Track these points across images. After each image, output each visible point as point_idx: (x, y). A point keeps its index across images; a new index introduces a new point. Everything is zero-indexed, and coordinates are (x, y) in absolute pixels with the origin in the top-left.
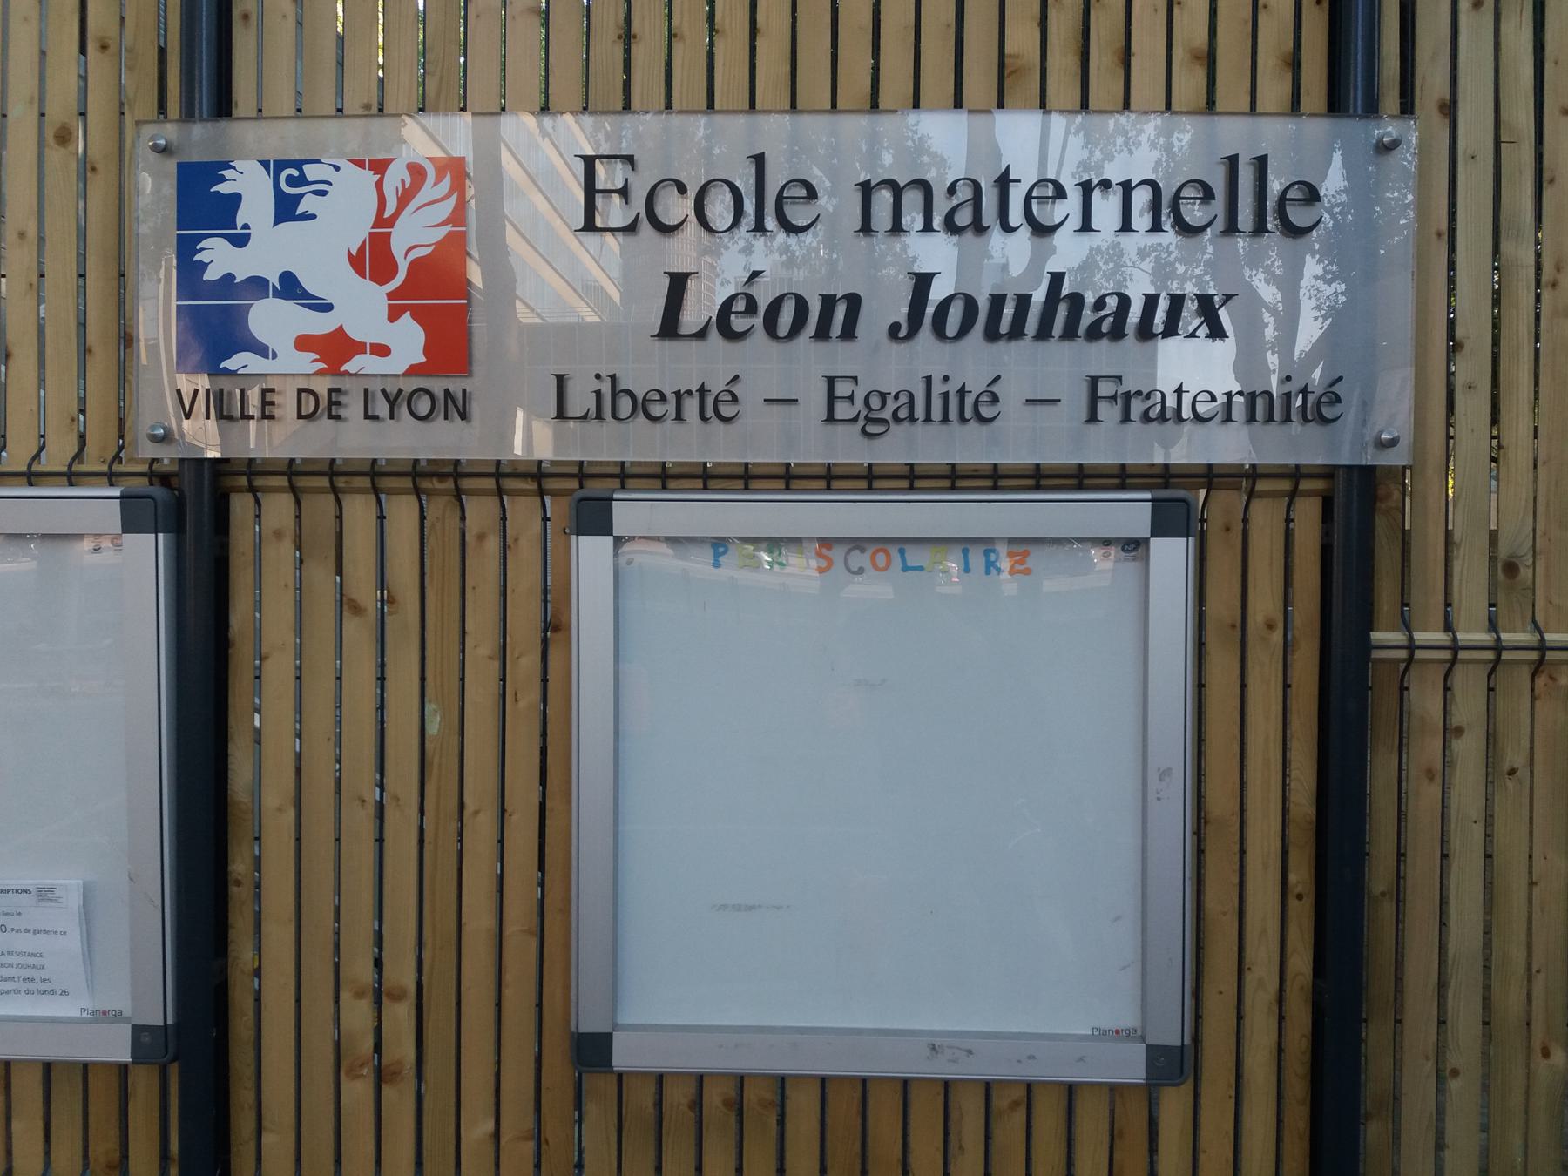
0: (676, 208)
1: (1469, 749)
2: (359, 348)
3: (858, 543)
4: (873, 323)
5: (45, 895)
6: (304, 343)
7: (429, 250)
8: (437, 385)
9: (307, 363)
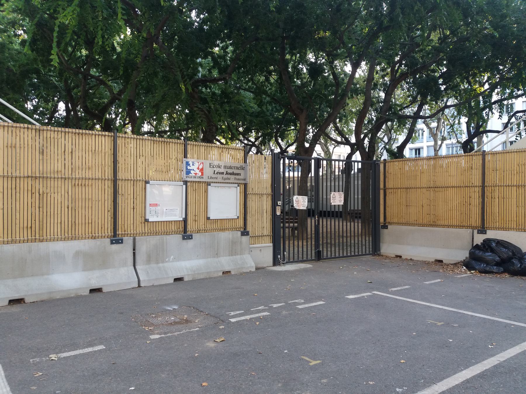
0: (214, 166)
1: (251, 199)
2: (197, 174)
3: (223, 187)
4: (224, 174)
5: (177, 209)
6: (194, 173)
7: (322, 158)
8: (202, 176)
9: (194, 175)
